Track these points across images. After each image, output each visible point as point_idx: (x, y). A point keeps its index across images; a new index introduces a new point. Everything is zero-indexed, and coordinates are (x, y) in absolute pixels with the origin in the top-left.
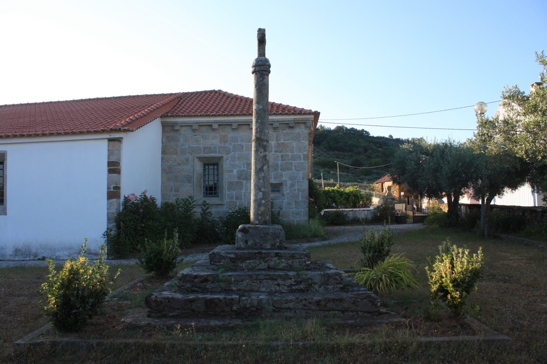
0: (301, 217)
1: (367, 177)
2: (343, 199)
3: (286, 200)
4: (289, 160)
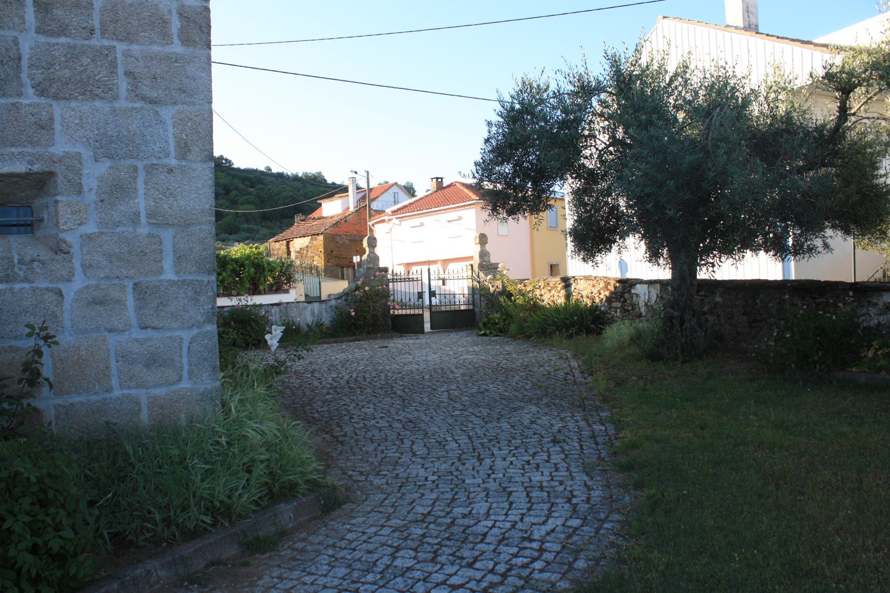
0: (180, 380)
1: (233, 236)
2: (229, 273)
3: (78, 282)
4: (92, 32)
